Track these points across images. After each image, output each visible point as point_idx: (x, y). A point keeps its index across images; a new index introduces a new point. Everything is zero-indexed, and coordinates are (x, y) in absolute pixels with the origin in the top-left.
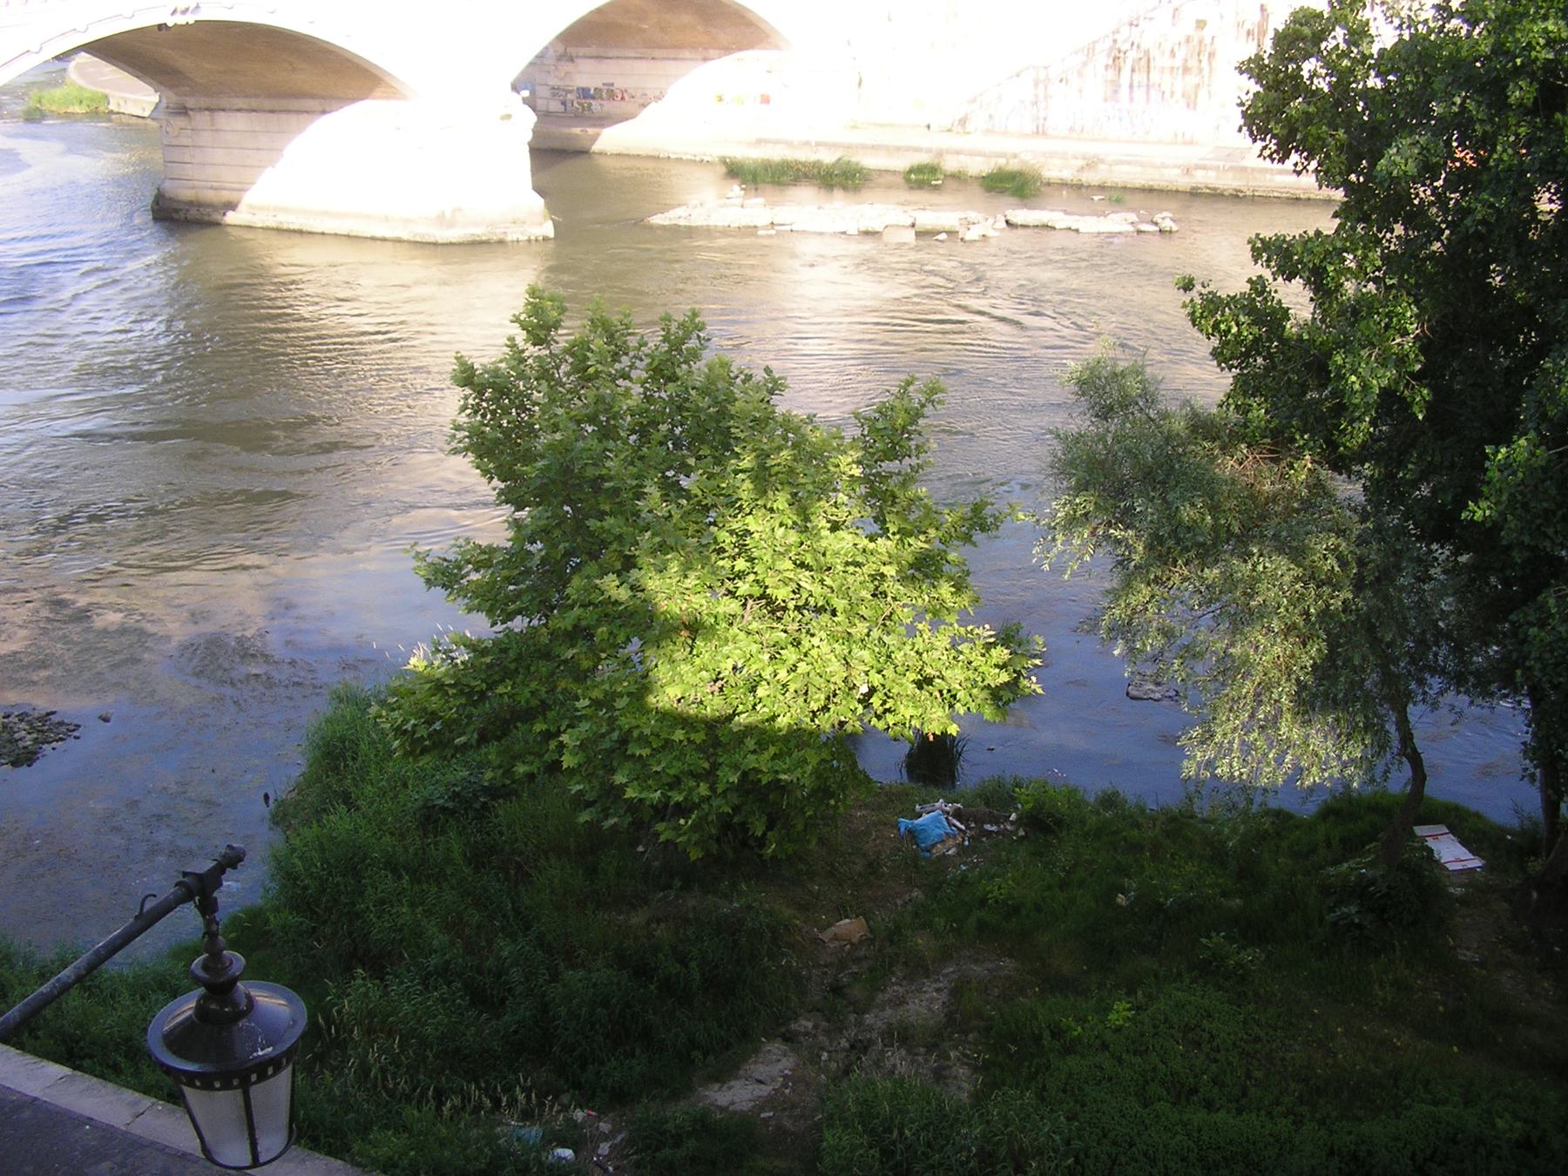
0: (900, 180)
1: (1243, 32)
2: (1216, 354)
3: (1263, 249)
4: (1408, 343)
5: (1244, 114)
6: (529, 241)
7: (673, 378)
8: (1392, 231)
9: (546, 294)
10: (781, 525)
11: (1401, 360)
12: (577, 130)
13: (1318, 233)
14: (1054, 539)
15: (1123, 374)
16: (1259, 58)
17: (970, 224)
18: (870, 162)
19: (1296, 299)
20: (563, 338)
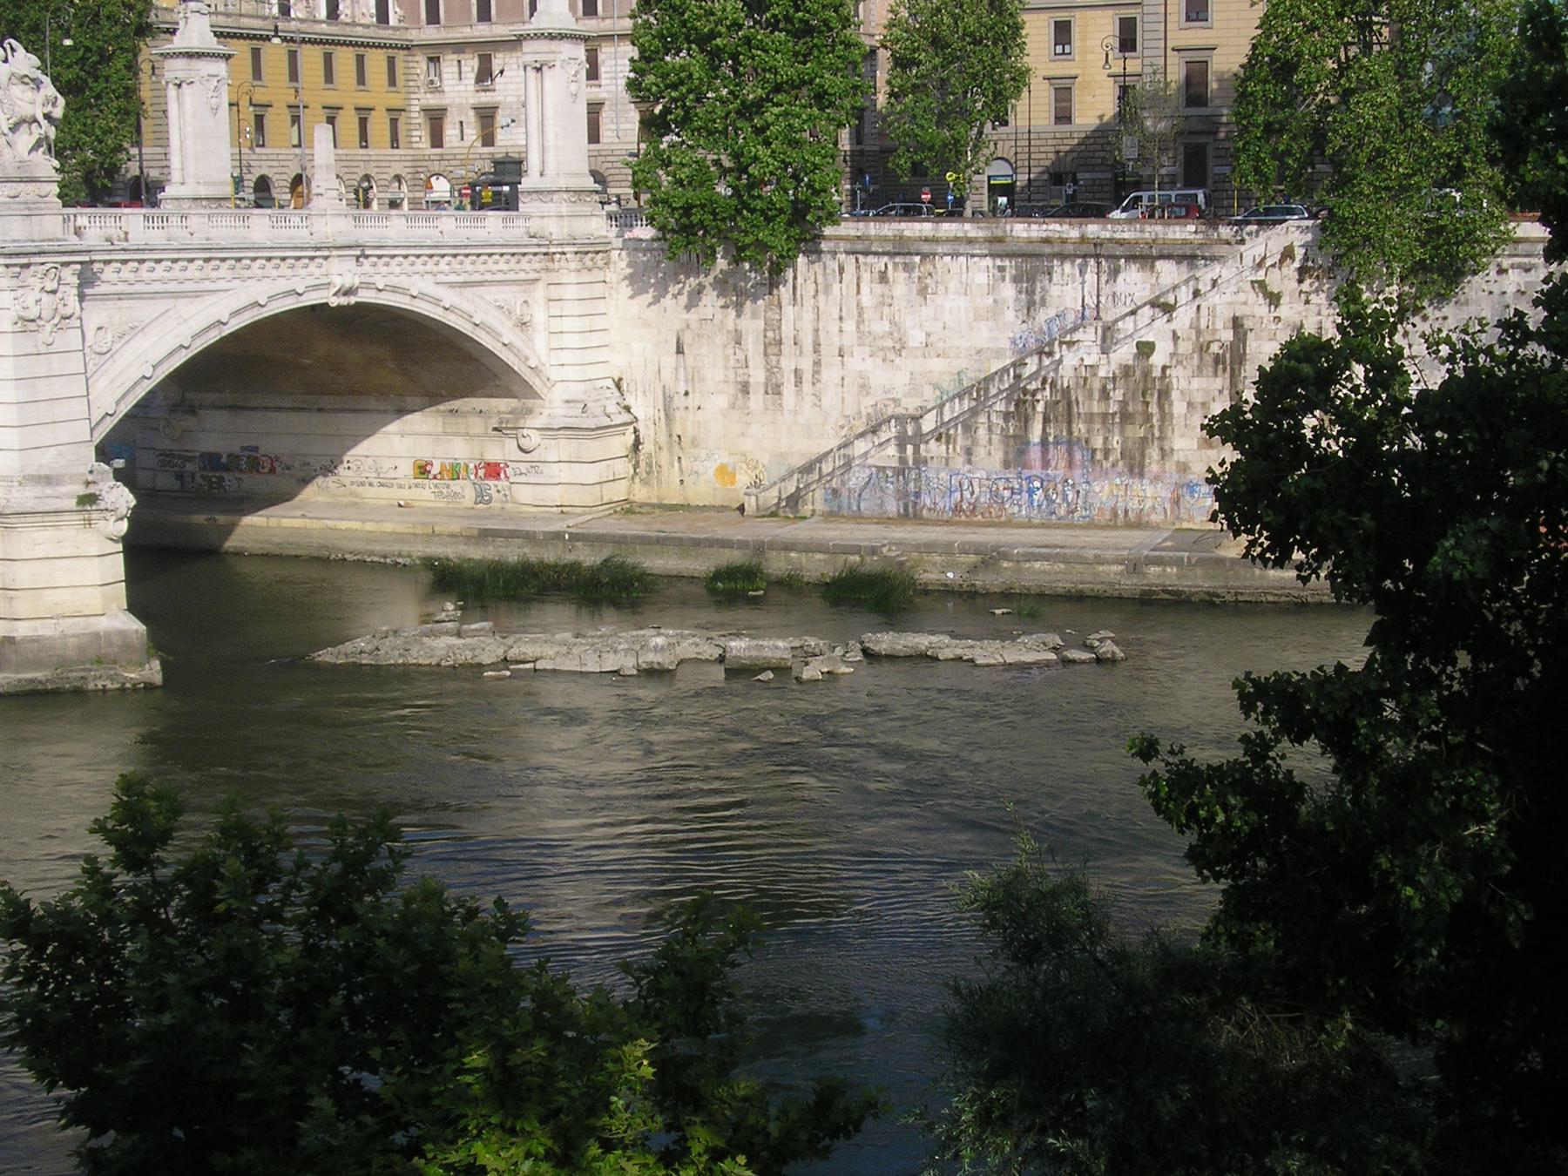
0: (699, 590)
1: (1209, 359)
2: (1195, 856)
3: (1257, 694)
4: (1489, 830)
5: (1218, 495)
6: (123, 690)
7: (349, 918)
8: (1454, 662)
9: (148, 789)
10: (528, 1155)
11: (1481, 858)
12: (200, 519)
13: (1340, 668)
14: (957, 1156)
15: (1055, 894)
16: (1236, 410)
17: (807, 655)
18: (657, 563)
19: (1308, 762)
20: (171, 858)
